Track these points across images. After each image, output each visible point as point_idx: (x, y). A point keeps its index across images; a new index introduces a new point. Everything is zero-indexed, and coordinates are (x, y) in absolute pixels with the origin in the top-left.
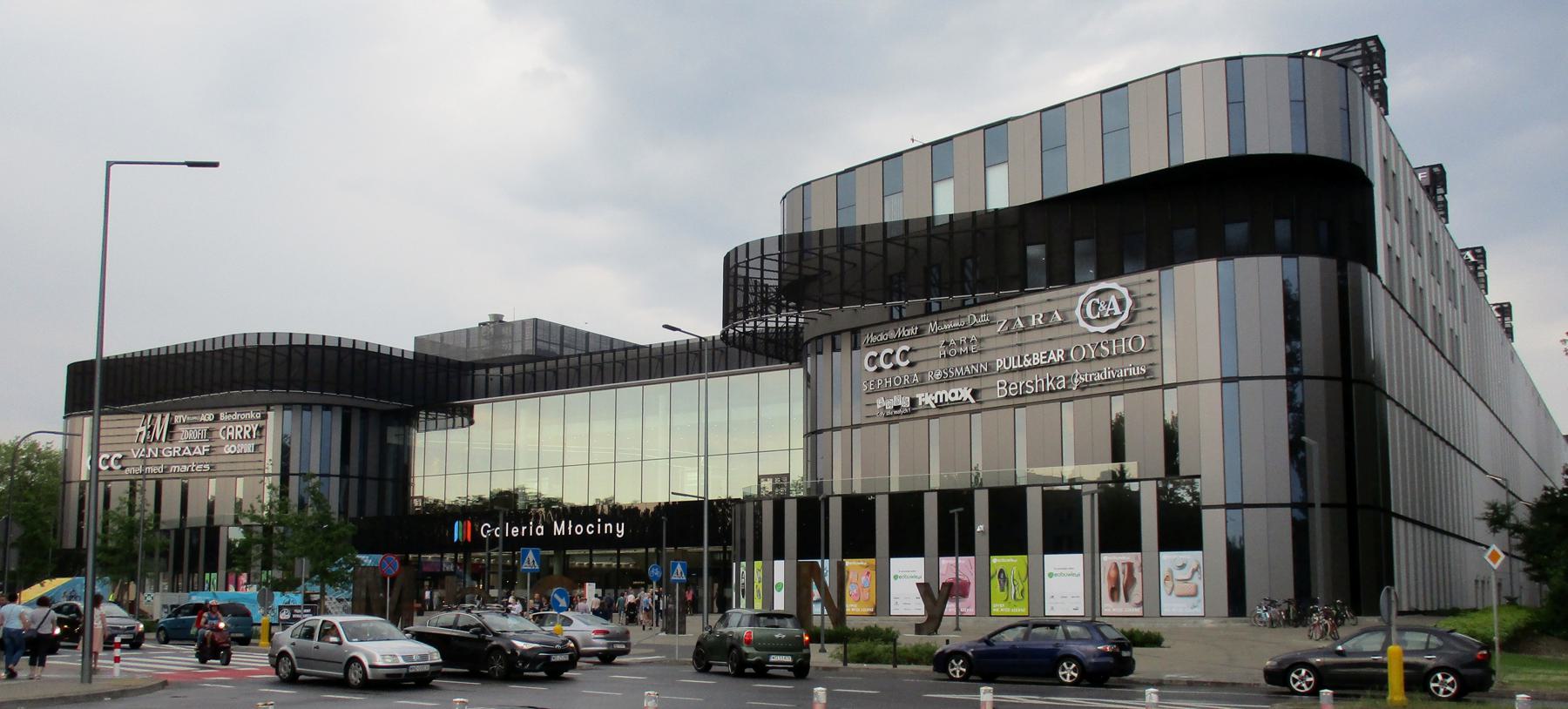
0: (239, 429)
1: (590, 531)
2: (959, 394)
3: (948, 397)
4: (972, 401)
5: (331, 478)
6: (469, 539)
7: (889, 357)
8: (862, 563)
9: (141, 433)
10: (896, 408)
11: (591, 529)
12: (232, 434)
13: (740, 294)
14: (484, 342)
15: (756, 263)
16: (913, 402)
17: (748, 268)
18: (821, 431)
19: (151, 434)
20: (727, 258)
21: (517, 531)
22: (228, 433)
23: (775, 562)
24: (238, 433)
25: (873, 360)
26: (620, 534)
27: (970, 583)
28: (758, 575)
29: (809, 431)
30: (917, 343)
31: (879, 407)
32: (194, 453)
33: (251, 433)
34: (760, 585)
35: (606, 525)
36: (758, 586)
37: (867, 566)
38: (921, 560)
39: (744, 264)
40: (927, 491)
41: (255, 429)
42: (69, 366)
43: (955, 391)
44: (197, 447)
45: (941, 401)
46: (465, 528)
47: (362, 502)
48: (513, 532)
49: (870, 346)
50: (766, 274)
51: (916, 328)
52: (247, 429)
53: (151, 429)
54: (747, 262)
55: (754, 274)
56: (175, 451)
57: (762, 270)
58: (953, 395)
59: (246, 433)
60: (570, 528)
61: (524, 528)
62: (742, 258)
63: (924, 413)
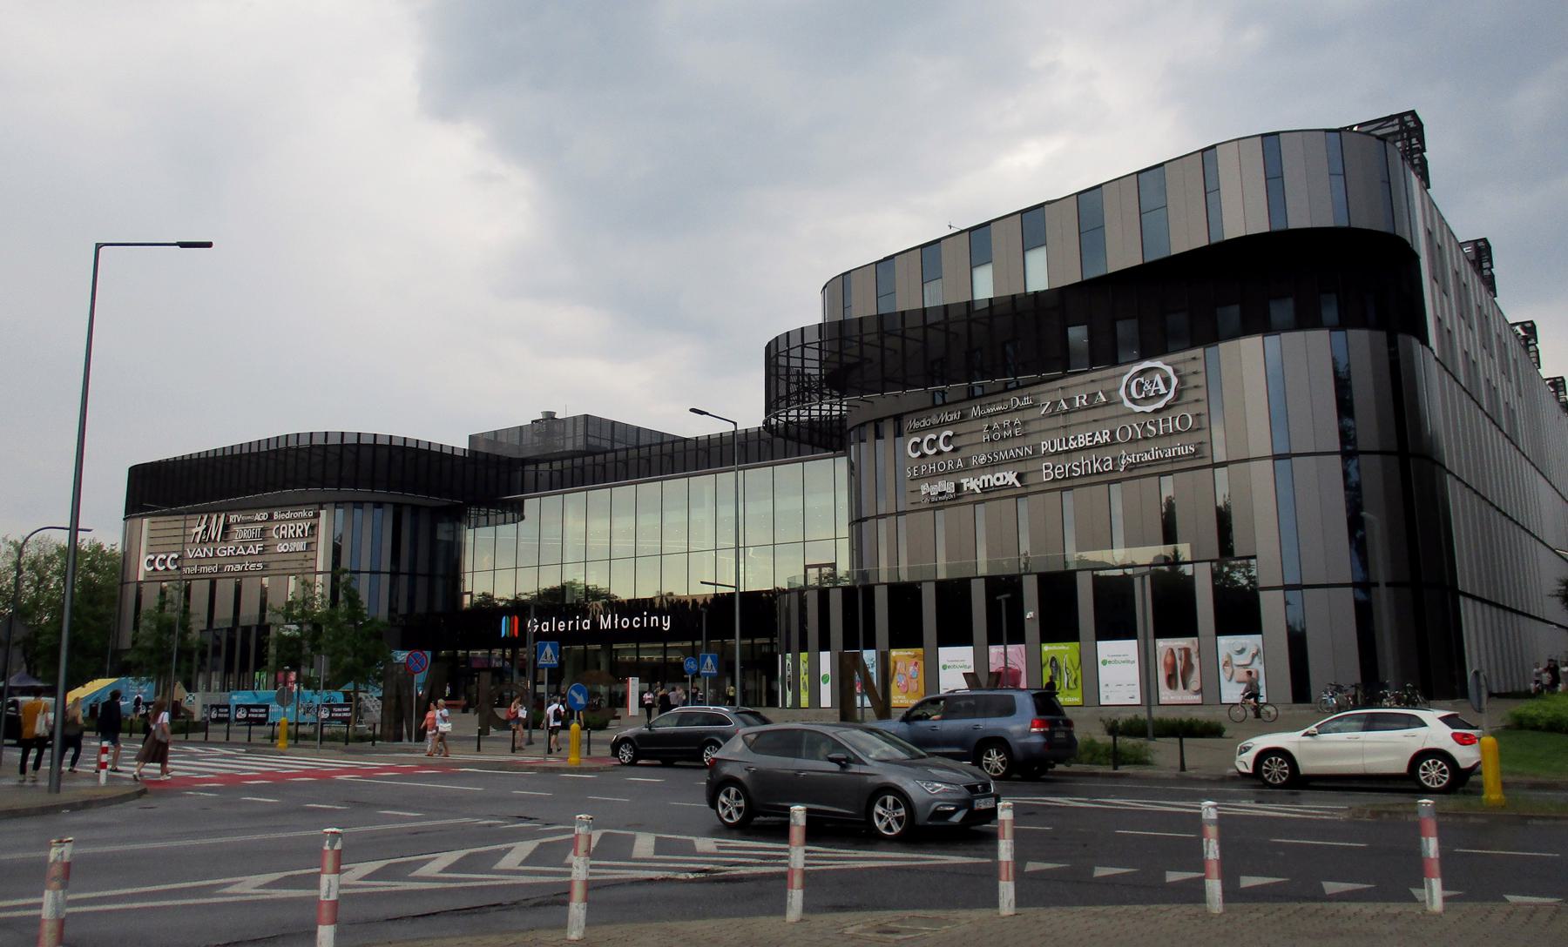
0: (292, 528)
1: (636, 624)
2: (1004, 478)
3: (993, 481)
4: (1018, 485)
5: (361, 574)
6: (517, 635)
7: (932, 443)
8: (909, 653)
9: (197, 533)
10: (941, 494)
11: (637, 622)
12: (285, 532)
13: (782, 385)
14: (536, 439)
15: (796, 352)
16: (958, 487)
17: (788, 357)
18: (866, 519)
19: (206, 534)
20: (768, 348)
21: (564, 625)
22: (282, 532)
23: (821, 653)
24: (291, 531)
25: (916, 446)
26: (666, 627)
27: (1021, 672)
28: (804, 667)
29: (854, 519)
30: (961, 428)
31: (923, 493)
32: (248, 552)
33: (303, 532)
34: (806, 678)
35: (652, 618)
36: (804, 678)
37: (915, 657)
38: (970, 649)
39: (817, 346)
40: (974, 578)
41: (307, 528)
42: (130, 469)
43: (1000, 475)
44: (251, 546)
45: (986, 485)
46: (512, 623)
47: (411, 599)
48: (559, 626)
49: (915, 432)
50: (807, 363)
51: (959, 413)
52: (300, 527)
53: (206, 529)
54: (788, 351)
55: (795, 363)
56: (229, 551)
57: (803, 358)
58: (998, 479)
59: (299, 531)
60: (616, 622)
61: (570, 623)
62: (783, 347)
63: (970, 499)
